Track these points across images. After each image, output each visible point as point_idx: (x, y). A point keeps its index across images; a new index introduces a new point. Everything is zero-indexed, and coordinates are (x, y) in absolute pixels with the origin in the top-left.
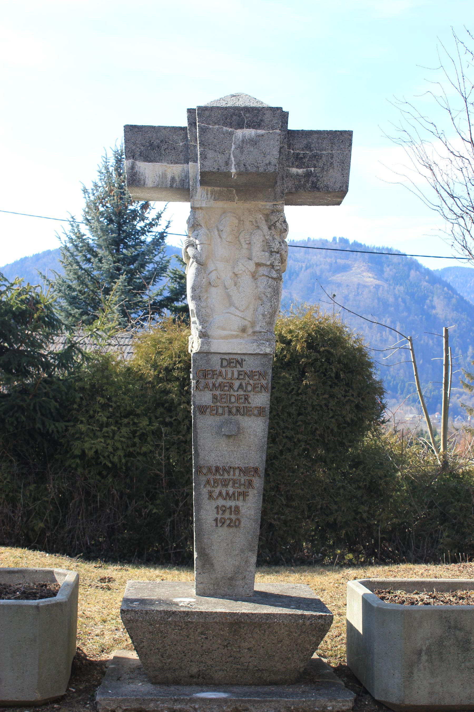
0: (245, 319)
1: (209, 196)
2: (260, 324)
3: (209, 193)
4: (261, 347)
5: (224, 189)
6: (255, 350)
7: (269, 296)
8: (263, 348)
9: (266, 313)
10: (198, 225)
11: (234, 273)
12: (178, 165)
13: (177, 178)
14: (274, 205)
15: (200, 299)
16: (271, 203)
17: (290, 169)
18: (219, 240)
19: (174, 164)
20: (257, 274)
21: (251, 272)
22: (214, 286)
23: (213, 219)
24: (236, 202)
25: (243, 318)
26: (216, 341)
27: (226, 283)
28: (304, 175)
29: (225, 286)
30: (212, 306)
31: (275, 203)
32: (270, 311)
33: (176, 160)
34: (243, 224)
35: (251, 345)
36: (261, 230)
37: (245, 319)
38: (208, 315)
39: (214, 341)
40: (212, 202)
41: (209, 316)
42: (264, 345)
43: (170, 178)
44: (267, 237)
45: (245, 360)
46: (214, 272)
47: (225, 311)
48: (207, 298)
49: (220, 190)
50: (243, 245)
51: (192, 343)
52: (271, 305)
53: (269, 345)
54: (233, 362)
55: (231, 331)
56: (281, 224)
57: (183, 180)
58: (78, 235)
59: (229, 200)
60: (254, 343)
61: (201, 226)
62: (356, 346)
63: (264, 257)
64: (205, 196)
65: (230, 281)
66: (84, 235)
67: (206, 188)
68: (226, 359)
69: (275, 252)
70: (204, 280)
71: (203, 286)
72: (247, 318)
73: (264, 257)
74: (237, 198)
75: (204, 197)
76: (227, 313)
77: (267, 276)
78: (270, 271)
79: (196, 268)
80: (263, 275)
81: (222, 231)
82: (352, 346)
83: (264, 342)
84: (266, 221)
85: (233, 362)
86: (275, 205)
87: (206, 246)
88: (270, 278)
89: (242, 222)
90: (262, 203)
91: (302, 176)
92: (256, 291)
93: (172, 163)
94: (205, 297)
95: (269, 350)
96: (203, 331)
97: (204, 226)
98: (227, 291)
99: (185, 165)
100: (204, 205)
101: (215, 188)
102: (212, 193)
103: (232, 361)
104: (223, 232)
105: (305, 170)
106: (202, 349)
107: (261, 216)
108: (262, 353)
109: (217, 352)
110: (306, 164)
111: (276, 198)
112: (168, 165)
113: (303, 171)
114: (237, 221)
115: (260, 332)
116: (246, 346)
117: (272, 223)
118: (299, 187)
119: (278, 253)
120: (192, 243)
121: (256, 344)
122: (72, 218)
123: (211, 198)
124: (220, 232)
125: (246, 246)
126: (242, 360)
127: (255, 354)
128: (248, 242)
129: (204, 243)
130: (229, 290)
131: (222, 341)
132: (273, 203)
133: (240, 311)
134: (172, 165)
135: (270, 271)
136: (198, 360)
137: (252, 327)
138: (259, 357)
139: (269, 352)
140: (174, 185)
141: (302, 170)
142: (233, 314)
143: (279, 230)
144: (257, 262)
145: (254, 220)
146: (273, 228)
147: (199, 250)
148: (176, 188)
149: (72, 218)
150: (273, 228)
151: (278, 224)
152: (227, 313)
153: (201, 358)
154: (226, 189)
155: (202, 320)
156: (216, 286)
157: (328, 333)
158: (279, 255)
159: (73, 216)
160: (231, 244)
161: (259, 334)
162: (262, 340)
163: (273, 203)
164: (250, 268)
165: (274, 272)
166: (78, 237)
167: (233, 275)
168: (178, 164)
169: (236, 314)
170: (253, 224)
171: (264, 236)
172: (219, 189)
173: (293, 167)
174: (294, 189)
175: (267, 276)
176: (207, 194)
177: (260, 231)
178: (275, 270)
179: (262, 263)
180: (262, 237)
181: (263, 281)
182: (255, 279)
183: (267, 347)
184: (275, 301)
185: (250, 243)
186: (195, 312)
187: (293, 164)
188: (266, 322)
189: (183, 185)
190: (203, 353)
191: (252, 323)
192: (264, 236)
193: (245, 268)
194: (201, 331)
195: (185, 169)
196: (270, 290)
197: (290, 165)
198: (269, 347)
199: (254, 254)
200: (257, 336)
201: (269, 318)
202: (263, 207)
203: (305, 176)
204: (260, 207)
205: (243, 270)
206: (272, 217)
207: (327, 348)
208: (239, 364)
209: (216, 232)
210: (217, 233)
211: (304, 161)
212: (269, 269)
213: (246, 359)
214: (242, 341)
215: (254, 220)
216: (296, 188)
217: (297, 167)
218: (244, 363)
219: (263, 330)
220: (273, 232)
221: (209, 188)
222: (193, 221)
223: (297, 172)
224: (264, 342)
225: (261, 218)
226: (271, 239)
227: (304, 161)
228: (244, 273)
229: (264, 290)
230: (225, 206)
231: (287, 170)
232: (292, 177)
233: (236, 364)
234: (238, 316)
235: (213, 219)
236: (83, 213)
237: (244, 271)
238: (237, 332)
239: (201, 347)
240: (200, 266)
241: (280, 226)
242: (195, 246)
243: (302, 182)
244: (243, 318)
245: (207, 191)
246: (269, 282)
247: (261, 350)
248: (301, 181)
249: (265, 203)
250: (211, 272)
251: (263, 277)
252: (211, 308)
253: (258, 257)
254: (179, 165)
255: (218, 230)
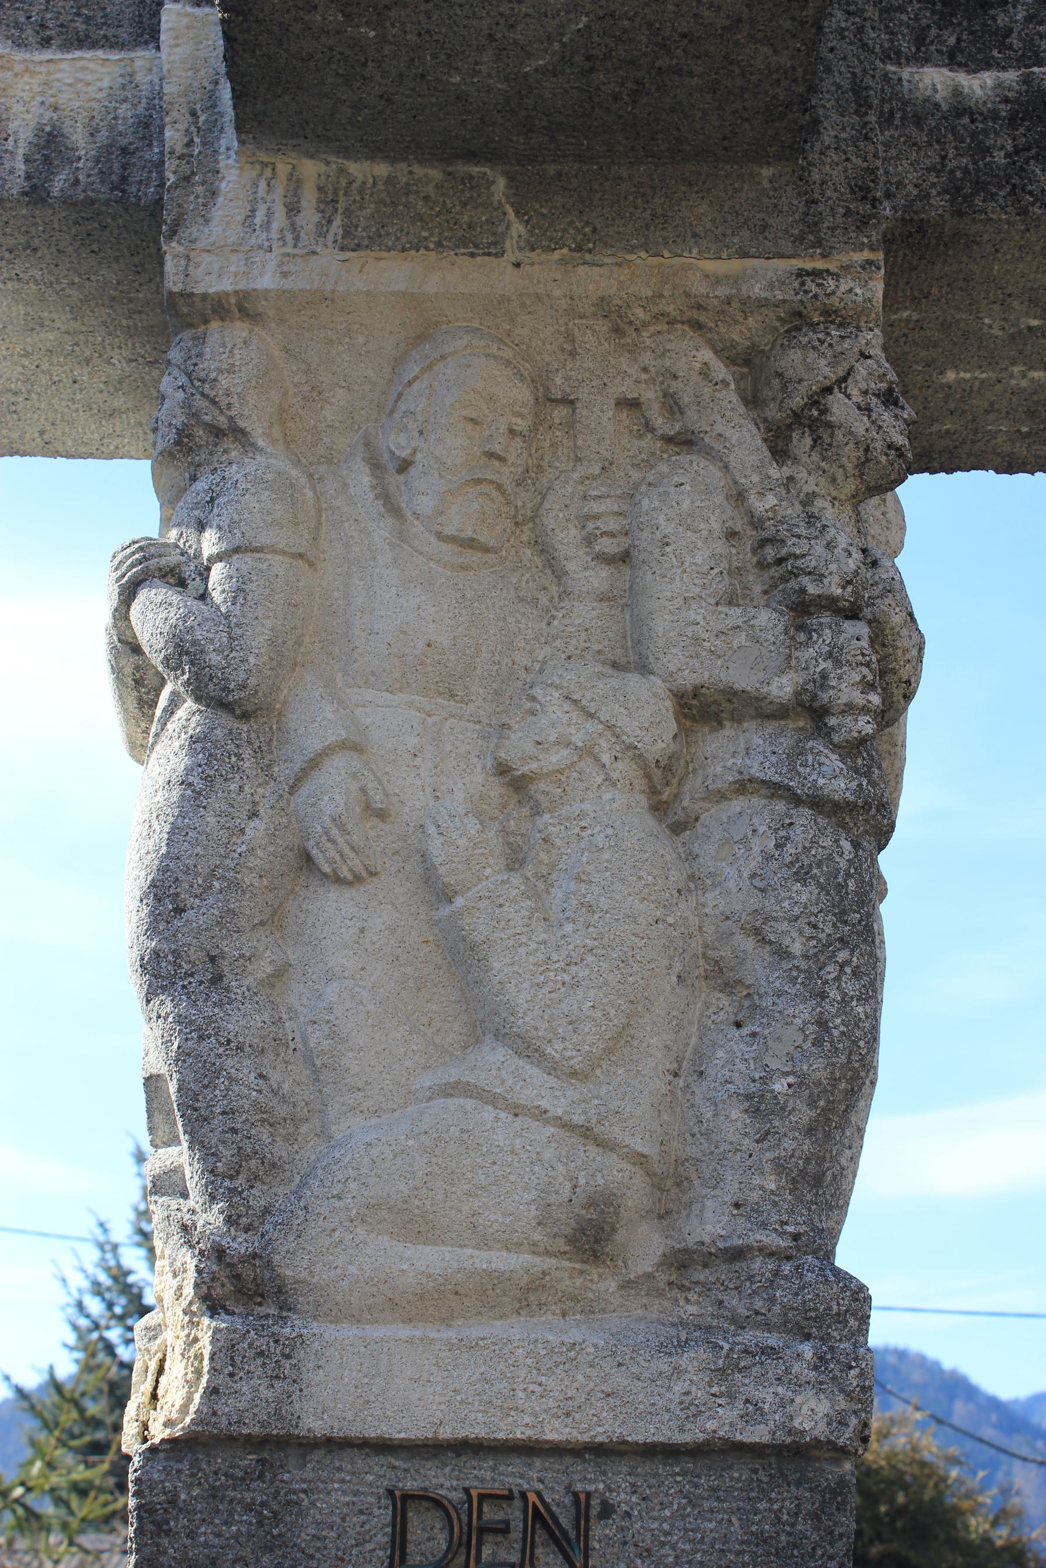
0: (603, 1144)
1: (309, 217)
2: (731, 1189)
3: (309, 198)
4: (746, 1385)
5: (419, 171)
6: (692, 1411)
7: (797, 948)
8: (767, 1396)
9: (780, 1086)
10: (218, 433)
11: (502, 769)
12: (89, 54)
13: (78, 137)
14: (801, 273)
15: (217, 979)
16: (782, 265)
17: (906, 73)
18: (382, 531)
19: (65, 47)
20: (693, 786)
21: (639, 758)
22: (339, 881)
23: (340, 396)
24: (510, 256)
25: (586, 1132)
26: (348, 1332)
27: (436, 847)
28: (1004, 110)
29: (429, 875)
30: (316, 1037)
31: (809, 265)
32: (817, 1069)
33: (81, 27)
34: (570, 426)
35: (663, 1364)
36: (709, 453)
37: (603, 1144)
38: (282, 1110)
39: (330, 1332)
40: (329, 259)
41: (295, 1121)
42: (774, 1368)
43: (26, 135)
44: (763, 504)
45: (607, 1511)
46: (338, 766)
47: (427, 1080)
48: (280, 973)
49: (390, 181)
50: (571, 566)
51: (153, 1366)
52: (822, 1023)
53: (820, 1362)
54: (504, 1529)
55: (484, 1242)
56: (866, 410)
57: (124, 151)
58: (115, 1272)
59: (463, 242)
60: (683, 1346)
61: (239, 434)
62: (1001, 1535)
63: (741, 639)
64: (280, 220)
65: (472, 825)
66: (129, 1272)
67: (283, 169)
68: (438, 1503)
69: (830, 604)
70: (256, 829)
71: (248, 879)
72: (615, 1132)
73: (741, 639)
74: (518, 228)
75: (267, 225)
76: (449, 1090)
77: (775, 790)
78: (796, 753)
79: (194, 740)
80: (744, 786)
81: (404, 466)
82: (987, 1540)
83: (773, 1340)
84: (752, 401)
85: (504, 1529)
86: (816, 274)
87: (278, 564)
88: (797, 801)
89: (559, 413)
90: (710, 266)
91: (994, 115)
92: (685, 908)
93: (46, 43)
94: (263, 968)
95: (823, 1407)
96: (239, 1245)
97: (267, 435)
98: (445, 911)
99: (141, 56)
100: (267, 280)
101: (355, 168)
102: (328, 201)
103: (491, 1514)
104: (413, 471)
105: (1011, 76)
106: (226, 1407)
107: (706, 355)
108: (758, 1434)
109: (355, 1431)
110: (1015, 41)
111: (813, 227)
112: (20, 56)
113: (999, 85)
114: (522, 394)
115: (737, 1254)
116: (620, 1380)
117: (797, 401)
118: (979, 186)
119: (853, 614)
120: (174, 558)
121: (703, 1354)
122: (102, 1225)
123: (321, 232)
124: (394, 480)
125: (599, 578)
126: (581, 1504)
127: (697, 1451)
128: (608, 546)
129: (263, 539)
130: (459, 902)
131: (405, 1332)
132: (796, 264)
133: (553, 1068)
134: (48, 55)
135: (796, 753)
136: (187, 1510)
137: (664, 1215)
138: (739, 1473)
139: (821, 1431)
140: (58, 184)
141: (988, 77)
142: (492, 1100)
143: (850, 454)
144: (688, 679)
145: (650, 395)
146: (802, 443)
147: (217, 597)
148: (68, 202)
149: (102, 1225)
150: (802, 443)
151: (840, 408)
152: (449, 1090)
153: (214, 1494)
154: (435, 174)
155: (227, 1153)
156: (358, 879)
157: (897, 1481)
158: (862, 629)
159: (103, 1218)
160: (474, 557)
161: (722, 1271)
162: (757, 1320)
163: (796, 264)
164: (631, 727)
165: (833, 761)
166: (115, 1279)
167: (497, 790)
168: (94, 45)
169: (526, 1096)
170: (649, 428)
171: (739, 497)
172: (382, 169)
173: (927, 60)
174: (939, 203)
175: (775, 790)
176: (293, 209)
177: (697, 464)
178: (836, 747)
179: (731, 694)
180: (719, 498)
181: (741, 829)
182: (677, 829)
183: (800, 1385)
184: (851, 987)
185: (625, 557)
186: (173, 1087)
187: (920, 40)
188: (780, 1166)
189: (124, 179)
190: (230, 1440)
191: (658, 1184)
192: (739, 497)
193: (590, 726)
194: (220, 1253)
195: (141, 78)
196: (805, 894)
197: (905, 46)
198: (819, 1388)
199: (661, 625)
200: (707, 1289)
201: (810, 1131)
202: (722, 291)
203: (1013, 120)
204: (699, 288)
205: (578, 739)
206: (792, 360)
207: (894, 1546)
208: (560, 1542)
209: (362, 479)
210: (366, 480)
211: (1002, 20)
212: (786, 743)
213: (622, 1498)
214: (574, 1335)
215: (650, 395)
216: (953, 190)
217: (953, 60)
218: (598, 1530)
219: (762, 1237)
220: (802, 474)
221: (311, 169)
222: (186, 405)
223: (957, 92)
224: (773, 1340)
225: (705, 372)
226: (793, 511)
227: (1002, 20)
228: (587, 765)
229: (755, 902)
230: (432, 285)
231: (886, 78)
232: (918, 121)
233: (528, 1548)
234: (541, 1115)
235: (340, 396)
236: (132, 1216)
237: (588, 751)
238: (535, 1249)
239: (212, 1392)
240: (227, 720)
241: (860, 425)
242: (195, 585)
243: (999, 158)
244: (586, 1132)
245: (295, 183)
246: (800, 835)
247: (754, 1411)
248: (988, 151)
249: (736, 265)
250: (314, 764)
251: (737, 804)
252: (309, 1059)
253: (697, 640)
254: (100, 54)
255: (376, 466)
